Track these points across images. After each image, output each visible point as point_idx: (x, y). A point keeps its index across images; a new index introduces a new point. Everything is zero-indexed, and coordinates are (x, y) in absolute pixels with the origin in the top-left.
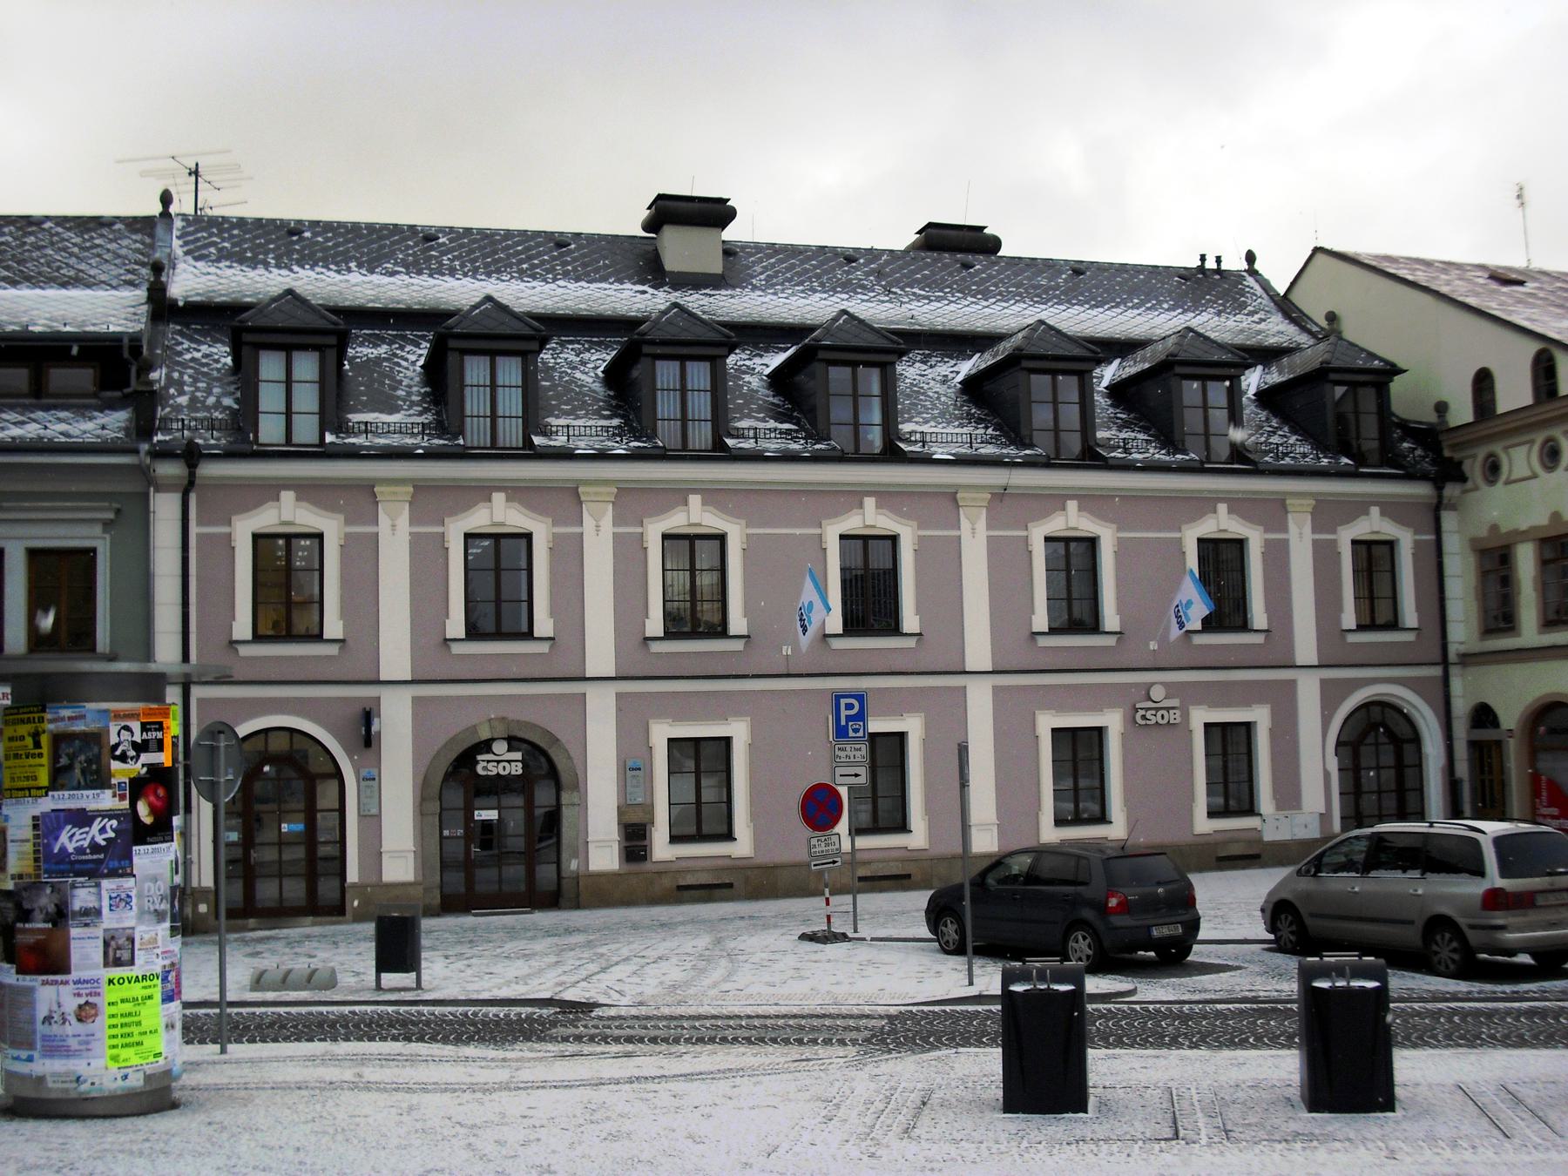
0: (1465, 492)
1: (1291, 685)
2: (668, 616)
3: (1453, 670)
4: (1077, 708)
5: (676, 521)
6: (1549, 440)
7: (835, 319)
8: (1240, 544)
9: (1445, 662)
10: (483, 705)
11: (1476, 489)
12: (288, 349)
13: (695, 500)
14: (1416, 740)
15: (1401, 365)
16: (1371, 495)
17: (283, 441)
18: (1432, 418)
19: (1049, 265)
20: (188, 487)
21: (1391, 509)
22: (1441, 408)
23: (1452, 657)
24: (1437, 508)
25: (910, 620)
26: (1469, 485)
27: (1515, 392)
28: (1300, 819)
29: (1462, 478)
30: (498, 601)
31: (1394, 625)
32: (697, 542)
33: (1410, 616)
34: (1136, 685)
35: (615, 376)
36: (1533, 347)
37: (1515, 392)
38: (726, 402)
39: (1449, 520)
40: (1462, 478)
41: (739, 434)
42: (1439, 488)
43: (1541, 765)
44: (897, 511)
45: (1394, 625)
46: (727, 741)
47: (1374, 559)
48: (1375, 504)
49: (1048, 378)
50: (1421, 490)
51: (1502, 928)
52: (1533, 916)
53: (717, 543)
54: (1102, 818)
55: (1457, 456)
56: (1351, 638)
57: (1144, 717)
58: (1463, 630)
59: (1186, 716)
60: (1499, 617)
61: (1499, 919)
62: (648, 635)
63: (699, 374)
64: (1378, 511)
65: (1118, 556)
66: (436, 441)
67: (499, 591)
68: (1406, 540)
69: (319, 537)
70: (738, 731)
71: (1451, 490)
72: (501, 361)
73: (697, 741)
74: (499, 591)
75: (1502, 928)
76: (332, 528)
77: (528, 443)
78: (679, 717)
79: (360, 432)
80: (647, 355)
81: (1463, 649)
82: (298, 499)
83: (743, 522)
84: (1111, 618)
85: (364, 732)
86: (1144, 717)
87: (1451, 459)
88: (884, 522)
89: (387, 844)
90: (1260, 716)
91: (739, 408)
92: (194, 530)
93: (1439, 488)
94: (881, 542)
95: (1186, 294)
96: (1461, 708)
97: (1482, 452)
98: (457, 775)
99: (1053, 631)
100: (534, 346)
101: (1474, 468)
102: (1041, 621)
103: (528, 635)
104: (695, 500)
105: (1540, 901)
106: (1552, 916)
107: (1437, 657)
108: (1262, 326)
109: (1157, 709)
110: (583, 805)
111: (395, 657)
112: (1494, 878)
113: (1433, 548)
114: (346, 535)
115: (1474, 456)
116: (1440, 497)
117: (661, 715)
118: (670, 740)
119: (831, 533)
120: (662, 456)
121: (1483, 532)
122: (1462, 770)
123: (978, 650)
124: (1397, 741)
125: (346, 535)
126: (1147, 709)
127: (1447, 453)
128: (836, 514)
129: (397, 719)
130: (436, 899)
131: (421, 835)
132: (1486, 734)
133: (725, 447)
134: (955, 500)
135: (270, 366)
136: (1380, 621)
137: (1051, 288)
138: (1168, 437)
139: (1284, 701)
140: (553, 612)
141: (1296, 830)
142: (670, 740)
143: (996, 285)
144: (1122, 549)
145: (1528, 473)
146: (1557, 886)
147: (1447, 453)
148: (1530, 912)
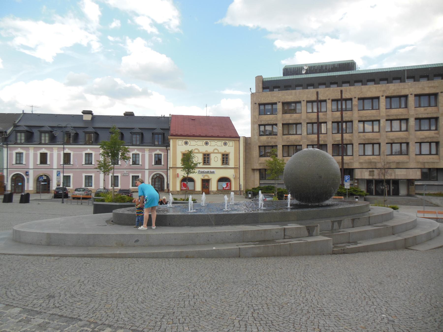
2: (133, 162)
5: (87, 152)
8: (70, 154)
9: (167, 169)
10: (41, 172)
12: (45, 133)
14: (164, 178)
20: (7, 147)
23: (168, 168)
25: (72, 163)
32: (428, 153)
44: (48, 150)
45: (91, 164)
50: (165, 148)
54: (91, 186)
65: (142, 156)
67: (44, 158)
70: (71, 175)
71: (168, 148)
74: (44, 158)
76: (24, 152)
78: (86, 173)
85: (27, 174)
89: (30, 186)
92: (9, 152)
98: (38, 180)
102: (84, 163)
103: (139, 164)
110: (52, 182)
111: (31, 166)
119: (84, 153)
123: (147, 167)
124: (161, 179)
128: (39, 150)
129: (31, 173)
130: (35, 192)
131: (34, 185)
135: (43, 135)
140: (26, 161)
144: (95, 155)
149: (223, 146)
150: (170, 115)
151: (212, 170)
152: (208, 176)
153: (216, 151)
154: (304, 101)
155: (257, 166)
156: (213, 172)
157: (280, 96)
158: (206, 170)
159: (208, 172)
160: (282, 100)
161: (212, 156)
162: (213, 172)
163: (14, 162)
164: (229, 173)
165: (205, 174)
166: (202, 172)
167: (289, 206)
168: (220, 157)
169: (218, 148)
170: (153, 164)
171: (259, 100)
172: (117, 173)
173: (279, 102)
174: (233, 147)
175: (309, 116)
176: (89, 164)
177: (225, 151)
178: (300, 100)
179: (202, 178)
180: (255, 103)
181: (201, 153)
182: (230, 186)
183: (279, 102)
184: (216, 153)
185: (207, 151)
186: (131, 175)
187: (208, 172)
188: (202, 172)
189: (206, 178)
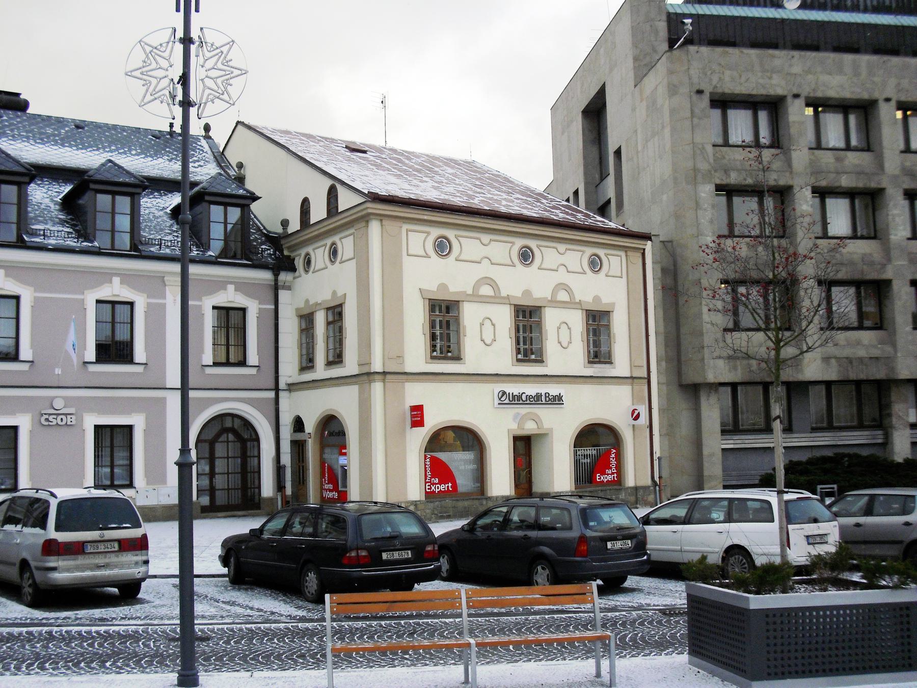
0: (294, 278)
1: (163, 401)
3: (281, 394)
4: (113, 412)
6: (333, 244)
7: (103, 165)
9: (277, 389)
11: (300, 276)
13: (116, 280)
14: (257, 439)
15: (258, 194)
16: (228, 277)
17: (109, 246)
18: (279, 230)
19: (60, 122)
21: (241, 287)
22: (285, 223)
23: (282, 385)
24: (276, 288)
26: (297, 274)
27: (318, 212)
28: (164, 490)
29: (293, 269)
30: (228, 345)
31: (242, 363)
33: (253, 357)
34: (47, 397)
35: (69, 204)
36: (328, 183)
37: (318, 212)
38: (27, 212)
39: (283, 295)
40: (293, 269)
41: (34, 233)
42: (276, 275)
43: (326, 456)
45: (242, 363)
46: (130, 428)
47: (231, 320)
48: (231, 283)
49: (109, 197)
50: (265, 276)
51: (54, 569)
52: (81, 560)
53: (14, 301)
55: (292, 255)
56: (209, 371)
57: (47, 420)
58: (289, 370)
59: (80, 420)
60: (307, 364)
61: (52, 562)
62: (204, 364)
63: (123, 203)
64: (231, 286)
66: (85, 244)
68: (253, 309)
69: (131, 304)
71: (284, 277)
72: (118, 198)
73: (112, 427)
75: (54, 569)
77: (20, 239)
79: (40, 235)
80: (93, 190)
81: (290, 381)
82: (236, 290)
83: (145, 295)
84: (26, 352)
86: (47, 420)
87: (289, 257)
88: (124, 293)
90: (138, 421)
91: (35, 218)
93: (276, 275)
94: (105, 305)
95: (152, 147)
96: (286, 420)
97: (303, 252)
99: (216, 364)
100: (27, 179)
101: (299, 263)
104: (116, 280)
105: (89, 549)
106: (100, 560)
107: (272, 386)
108: (199, 169)
109: (58, 415)
112: (52, 533)
113: (273, 314)
114: (35, 297)
115: (300, 255)
116: (276, 280)
117: (91, 410)
118: (96, 426)
120: (98, 253)
121: (302, 305)
122: (286, 459)
125: (35, 297)
126: (50, 414)
127: (286, 253)
132: (299, 436)
133: (23, 241)
134: (164, 282)
136: (232, 360)
137: (55, 135)
138: (84, 234)
139: (156, 410)
141: (161, 498)
142: (96, 426)
143: (12, 130)
144: (37, 305)
145: (323, 266)
146: (106, 538)
147: (286, 253)
148: (80, 557)
149: (519, 266)
150: (240, 166)
151: (553, 389)
152: (536, 420)
153: (486, 290)
154: (888, 100)
155: (718, 370)
156: (557, 400)
157: (796, 69)
158: (531, 389)
159: (536, 399)
160: (806, 91)
161: (551, 319)
162: (557, 400)
163: (208, 359)
164: (611, 405)
165: (524, 410)
166: (517, 400)
167: (465, 611)
168: (504, 318)
169: (569, 279)
170: (91, 354)
171: (715, 79)
172: (13, 413)
173: (796, 96)
174: (624, 280)
175: (908, 164)
176: (228, 364)
177: (443, 287)
178: (876, 95)
179: (514, 426)
180: (700, 92)
181: (506, 300)
182: (619, 467)
183: (796, 96)
184: (564, 305)
185: (597, 299)
186: (91, 421)
187: (538, 397)
188: (517, 400)
189: (530, 428)
